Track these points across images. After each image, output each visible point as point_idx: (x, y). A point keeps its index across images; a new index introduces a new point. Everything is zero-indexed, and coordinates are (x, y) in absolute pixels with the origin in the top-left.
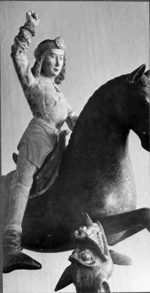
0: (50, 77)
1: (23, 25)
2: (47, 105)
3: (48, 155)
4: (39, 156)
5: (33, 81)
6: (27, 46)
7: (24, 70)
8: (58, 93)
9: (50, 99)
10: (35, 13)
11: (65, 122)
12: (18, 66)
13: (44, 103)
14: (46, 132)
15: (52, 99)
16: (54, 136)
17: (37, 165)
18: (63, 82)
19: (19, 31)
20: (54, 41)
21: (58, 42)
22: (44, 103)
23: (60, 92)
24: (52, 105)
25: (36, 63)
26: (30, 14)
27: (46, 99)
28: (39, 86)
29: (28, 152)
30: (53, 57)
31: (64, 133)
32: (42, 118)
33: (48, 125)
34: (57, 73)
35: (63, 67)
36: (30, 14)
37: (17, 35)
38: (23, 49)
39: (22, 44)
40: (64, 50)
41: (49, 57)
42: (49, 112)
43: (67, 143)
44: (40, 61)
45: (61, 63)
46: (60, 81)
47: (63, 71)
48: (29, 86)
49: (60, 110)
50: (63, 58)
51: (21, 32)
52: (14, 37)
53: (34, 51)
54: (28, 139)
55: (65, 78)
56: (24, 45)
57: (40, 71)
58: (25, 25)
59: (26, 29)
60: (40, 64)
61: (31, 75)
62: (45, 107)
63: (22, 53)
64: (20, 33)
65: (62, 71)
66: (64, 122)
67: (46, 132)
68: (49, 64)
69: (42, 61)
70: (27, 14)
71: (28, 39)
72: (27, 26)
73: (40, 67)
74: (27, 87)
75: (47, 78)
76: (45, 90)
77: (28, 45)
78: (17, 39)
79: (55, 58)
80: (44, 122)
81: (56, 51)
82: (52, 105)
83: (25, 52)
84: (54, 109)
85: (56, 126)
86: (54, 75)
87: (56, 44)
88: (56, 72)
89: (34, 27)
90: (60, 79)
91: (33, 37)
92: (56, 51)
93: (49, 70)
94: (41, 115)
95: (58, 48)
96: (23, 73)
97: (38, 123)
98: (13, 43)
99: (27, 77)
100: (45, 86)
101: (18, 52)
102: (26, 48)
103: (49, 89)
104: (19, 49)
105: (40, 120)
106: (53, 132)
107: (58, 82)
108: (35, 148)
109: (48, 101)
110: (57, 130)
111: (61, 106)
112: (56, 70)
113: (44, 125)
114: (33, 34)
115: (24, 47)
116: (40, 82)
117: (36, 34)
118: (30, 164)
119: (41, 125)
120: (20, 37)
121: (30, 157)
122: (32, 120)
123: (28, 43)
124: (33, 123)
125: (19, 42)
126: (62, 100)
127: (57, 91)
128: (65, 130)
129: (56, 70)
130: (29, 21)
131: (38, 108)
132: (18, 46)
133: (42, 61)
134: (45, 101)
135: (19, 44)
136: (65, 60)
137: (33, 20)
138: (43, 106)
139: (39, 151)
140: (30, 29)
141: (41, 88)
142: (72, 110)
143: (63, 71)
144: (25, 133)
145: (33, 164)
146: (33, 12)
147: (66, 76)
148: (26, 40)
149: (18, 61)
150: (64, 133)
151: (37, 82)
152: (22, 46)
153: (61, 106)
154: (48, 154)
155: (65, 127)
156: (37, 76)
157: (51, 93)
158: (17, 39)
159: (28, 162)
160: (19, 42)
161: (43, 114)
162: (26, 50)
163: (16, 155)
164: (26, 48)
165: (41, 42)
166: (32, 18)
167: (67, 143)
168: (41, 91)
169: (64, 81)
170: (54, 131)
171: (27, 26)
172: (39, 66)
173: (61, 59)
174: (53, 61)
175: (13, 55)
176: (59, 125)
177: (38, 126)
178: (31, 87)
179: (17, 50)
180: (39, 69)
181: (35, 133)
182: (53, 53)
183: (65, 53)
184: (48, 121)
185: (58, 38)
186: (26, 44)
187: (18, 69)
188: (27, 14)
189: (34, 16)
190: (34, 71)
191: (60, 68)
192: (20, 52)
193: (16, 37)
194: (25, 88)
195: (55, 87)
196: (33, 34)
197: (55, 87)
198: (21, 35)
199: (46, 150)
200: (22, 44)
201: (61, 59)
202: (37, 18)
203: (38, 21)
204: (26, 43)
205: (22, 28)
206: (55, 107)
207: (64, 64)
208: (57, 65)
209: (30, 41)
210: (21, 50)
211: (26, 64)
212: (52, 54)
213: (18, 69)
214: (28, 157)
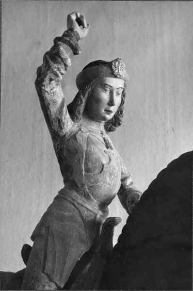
0: (98, 122)
1: (60, 35)
2: (88, 170)
3: (71, 274)
4: (65, 263)
5: (69, 125)
6: (63, 71)
7: (55, 110)
8: (109, 150)
9: (94, 161)
10: (82, 16)
11: (117, 196)
12: (45, 103)
13: (83, 166)
14: (82, 218)
15: (98, 160)
16: (93, 224)
17: (58, 283)
18: (118, 129)
19: (53, 44)
20: (109, 65)
21: (115, 66)
22: (83, 166)
23: (111, 149)
24: (97, 171)
25: (76, 96)
26: (74, 18)
27: (87, 159)
28: (77, 136)
29: (74, 205)
30: (106, 91)
31: (112, 222)
32: (77, 191)
33: (87, 205)
34: (109, 117)
35: (120, 106)
36: (74, 18)
37: (49, 49)
38: (57, 75)
39: (55, 66)
40: (125, 81)
41: (100, 89)
42: (90, 182)
43: (115, 242)
44: (84, 96)
45: (117, 100)
46: (113, 127)
47: (120, 111)
48: (61, 134)
49: (108, 179)
50: (121, 92)
51: (56, 46)
52: (44, 53)
53: (76, 77)
54: (48, 228)
55: (122, 124)
56: (59, 69)
57: (82, 111)
58: (64, 35)
59: (63, 42)
60: (84, 101)
61: (66, 117)
62: (84, 173)
63: (53, 82)
64: (53, 48)
65: (117, 112)
66: (114, 197)
67: (82, 218)
68: (98, 101)
69: (86, 95)
70: (69, 17)
71: (66, 59)
72: (68, 38)
73: (83, 105)
74: (58, 135)
75: (93, 123)
76: (87, 144)
77: (66, 69)
78: (48, 58)
79: (108, 92)
80: (80, 200)
81: (115, 83)
82: (97, 171)
83: (58, 81)
84: (100, 177)
85: (99, 206)
86: (104, 119)
87: (112, 70)
88: (109, 114)
89: (78, 39)
90: (112, 125)
91: (75, 56)
92: (115, 83)
93: (98, 110)
94: (77, 187)
95: (115, 77)
96: (53, 114)
97: (69, 199)
98: (40, 63)
99: (60, 121)
100: (88, 137)
101: (47, 80)
102: (62, 74)
103: (93, 143)
104: (50, 75)
105: (74, 194)
106: (93, 218)
107: (110, 128)
108: (58, 248)
109: (90, 164)
110: (100, 214)
111: (111, 174)
112: (108, 112)
113: (79, 204)
114: (75, 51)
115: (58, 72)
116: (80, 130)
117: (80, 52)
118: (47, 280)
119: (75, 203)
120: (53, 56)
121: (49, 265)
122: (62, 192)
123: (66, 65)
124: (61, 198)
125: (51, 63)
126: (113, 163)
127: (107, 147)
128: (114, 218)
129: (108, 112)
130: (71, 29)
131: (72, 172)
132: (48, 70)
133: (86, 95)
134: (86, 163)
135: (50, 66)
136: (124, 95)
137: (77, 28)
138: (81, 171)
139: (65, 254)
140: (71, 42)
141: (81, 140)
142: (128, 175)
143: (120, 111)
144: (45, 216)
145: (51, 281)
146: (79, 15)
147: (124, 119)
148: (63, 61)
149: (46, 93)
150: (112, 222)
151: (75, 128)
152: (55, 70)
153: (111, 174)
154: (71, 271)
155: (118, 211)
156: (77, 118)
157: (96, 150)
158: (48, 58)
159: (43, 275)
160: (51, 63)
161: (79, 185)
162: (61, 77)
163: (29, 246)
164: (62, 74)
165: (83, 68)
166: (77, 25)
167: (115, 242)
168: (81, 145)
169: (119, 127)
170: (97, 214)
171: (68, 38)
172: (82, 102)
173: (118, 94)
174: (105, 96)
175: (39, 84)
176: (104, 205)
177: (69, 205)
178: (64, 136)
179: (45, 76)
180: (82, 108)
181: (62, 218)
182: (107, 84)
183: (125, 85)
184: (87, 197)
185: (116, 60)
186: (62, 67)
187: (45, 107)
188: (69, 17)
189: (80, 22)
190: (72, 109)
191: (114, 109)
192: (51, 80)
193: (47, 53)
194: (57, 136)
195: (104, 139)
196: (75, 51)
197: (104, 139)
198: (54, 52)
199: (78, 250)
200: (55, 66)
201: (118, 94)
202: (86, 25)
203: (86, 31)
204: (63, 66)
205: (57, 40)
206: (101, 174)
207: (123, 102)
208: (111, 103)
209: (69, 62)
210: (53, 77)
211: (59, 101)
212: (104, 86)
213: (45, 107)
214: (44, 268)
